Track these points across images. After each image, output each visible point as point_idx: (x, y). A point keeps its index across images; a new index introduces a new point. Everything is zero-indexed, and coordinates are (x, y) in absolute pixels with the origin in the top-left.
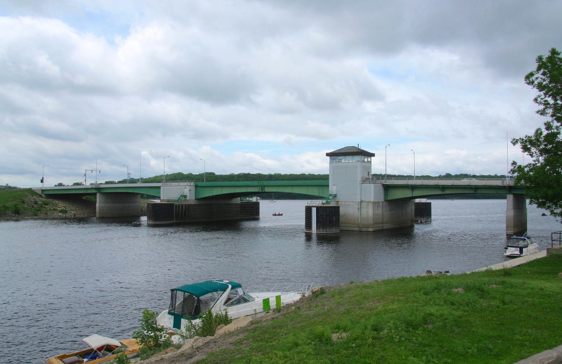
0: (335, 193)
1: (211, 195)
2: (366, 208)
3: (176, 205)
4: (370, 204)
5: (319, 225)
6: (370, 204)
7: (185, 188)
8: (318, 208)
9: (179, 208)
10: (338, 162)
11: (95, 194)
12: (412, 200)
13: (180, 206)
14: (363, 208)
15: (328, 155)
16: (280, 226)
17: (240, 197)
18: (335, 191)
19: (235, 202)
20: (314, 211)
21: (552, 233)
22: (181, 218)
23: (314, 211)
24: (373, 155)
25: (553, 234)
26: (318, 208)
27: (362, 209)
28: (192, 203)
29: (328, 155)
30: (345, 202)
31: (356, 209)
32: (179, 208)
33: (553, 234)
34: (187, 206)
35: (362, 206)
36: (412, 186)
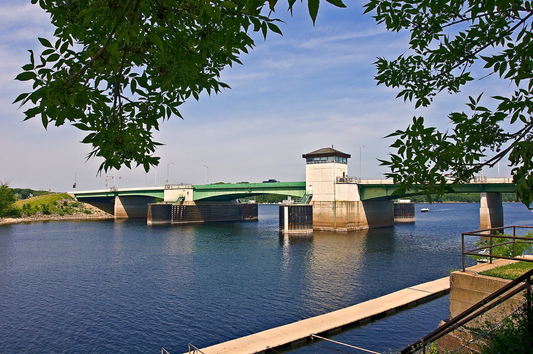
0: (311, 193)
1: (206, 197)
2: (340, 208)
3: (174, 206)
4: (344, 203)
5: (291, 223)
6: (344, 203)
7: (184, 191)
8: (290, 208)
9: (176, 209)
10: (314, 163)
11: (114, 198)
12: (391, 200)
13: (178, 207)
14: (338, 207)
15: (304, 156)
16: (304, 228)
17: (238, 198)
18: (311, 191)
19: (233, 203)
20: (286, 209)
21: (445, 35)
22: (179, 218)
23: (286, 209)
24: (349, 156)
25: (465, 236)
26: (290, 208)
27: (336, 208)
28: (190, 204)
29: (304, 156)
30: (321, 202)
31: (331, 208)
32: (176, 209)
33: (465, 236)
34: (185, 207)
35: (336, 206)
36: (386, 185)
